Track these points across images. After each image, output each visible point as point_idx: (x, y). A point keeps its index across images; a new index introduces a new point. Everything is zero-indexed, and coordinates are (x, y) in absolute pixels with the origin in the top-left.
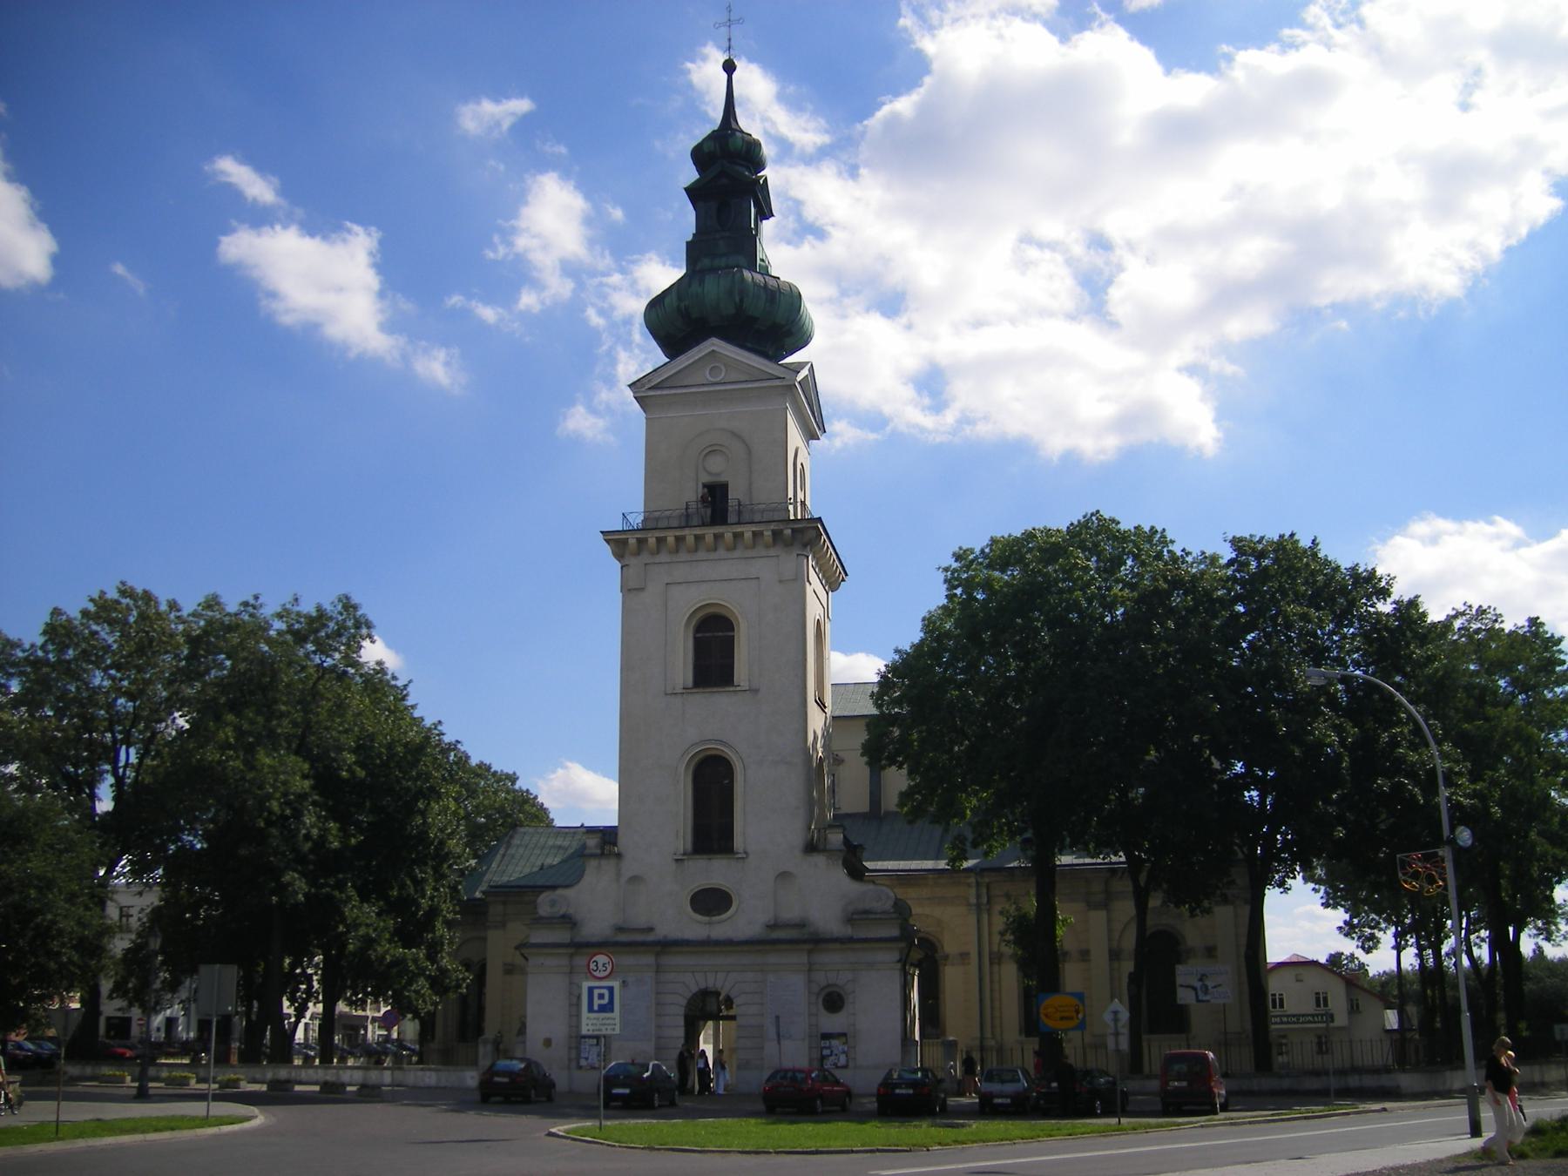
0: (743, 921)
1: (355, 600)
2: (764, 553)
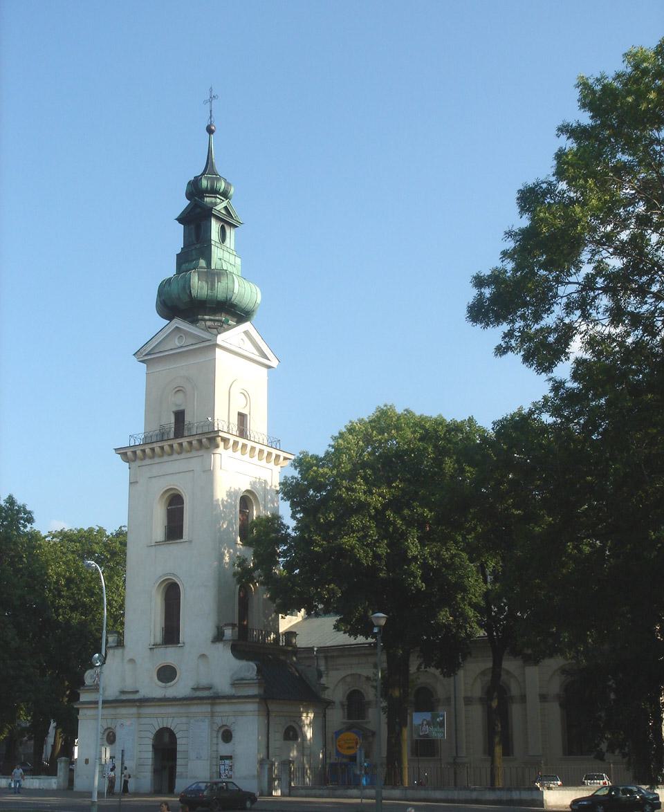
0: (181, 687)
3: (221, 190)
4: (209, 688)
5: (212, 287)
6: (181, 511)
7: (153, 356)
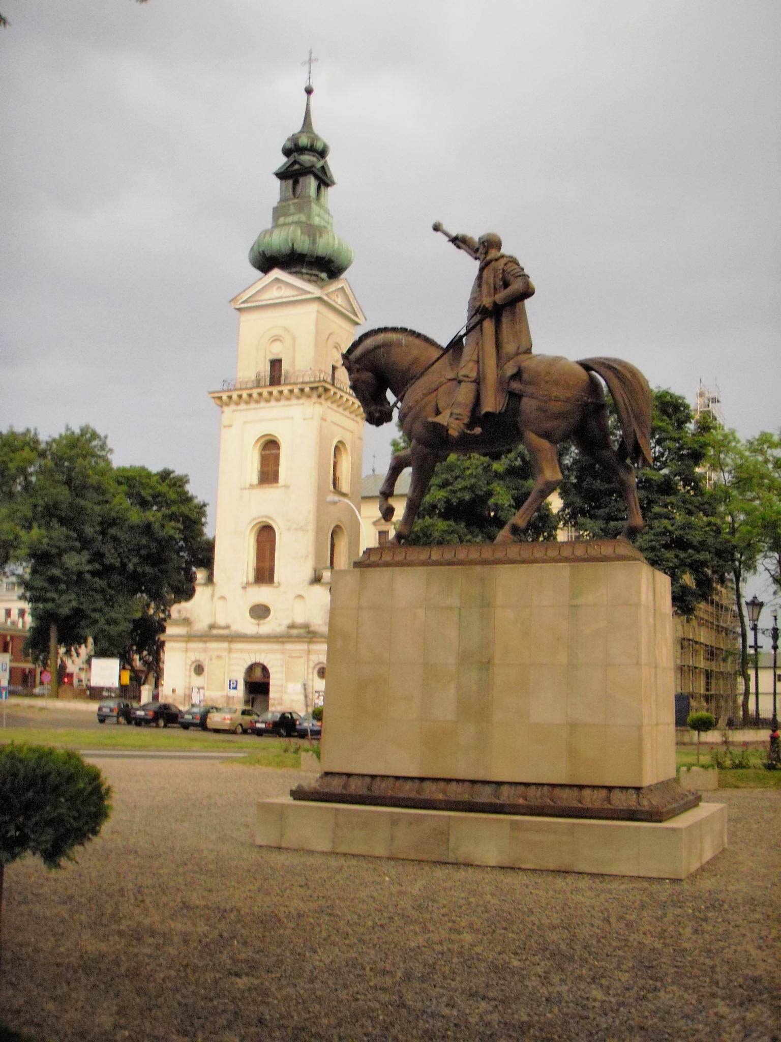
4: (228, 627)
5: (314, 242)
6: (277, 458)
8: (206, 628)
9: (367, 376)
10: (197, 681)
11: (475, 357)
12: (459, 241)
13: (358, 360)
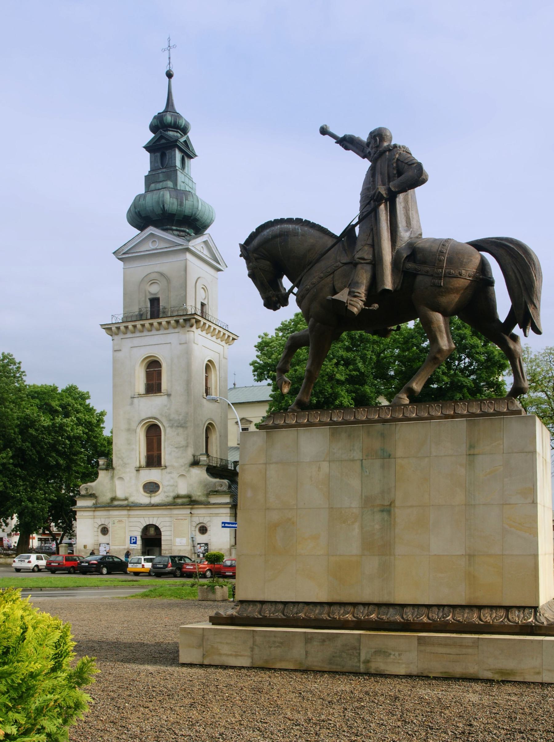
1: (251, 362)
2: (173, 331)
3: (182, 126)
4: (126, 499)
5: (181, 204)
7: (130, 255)
8: (109, 501)
9: (265, 264)
10: (103, 539)
11: (370, 242)
12: (347, 142)
13: (256, 250)
